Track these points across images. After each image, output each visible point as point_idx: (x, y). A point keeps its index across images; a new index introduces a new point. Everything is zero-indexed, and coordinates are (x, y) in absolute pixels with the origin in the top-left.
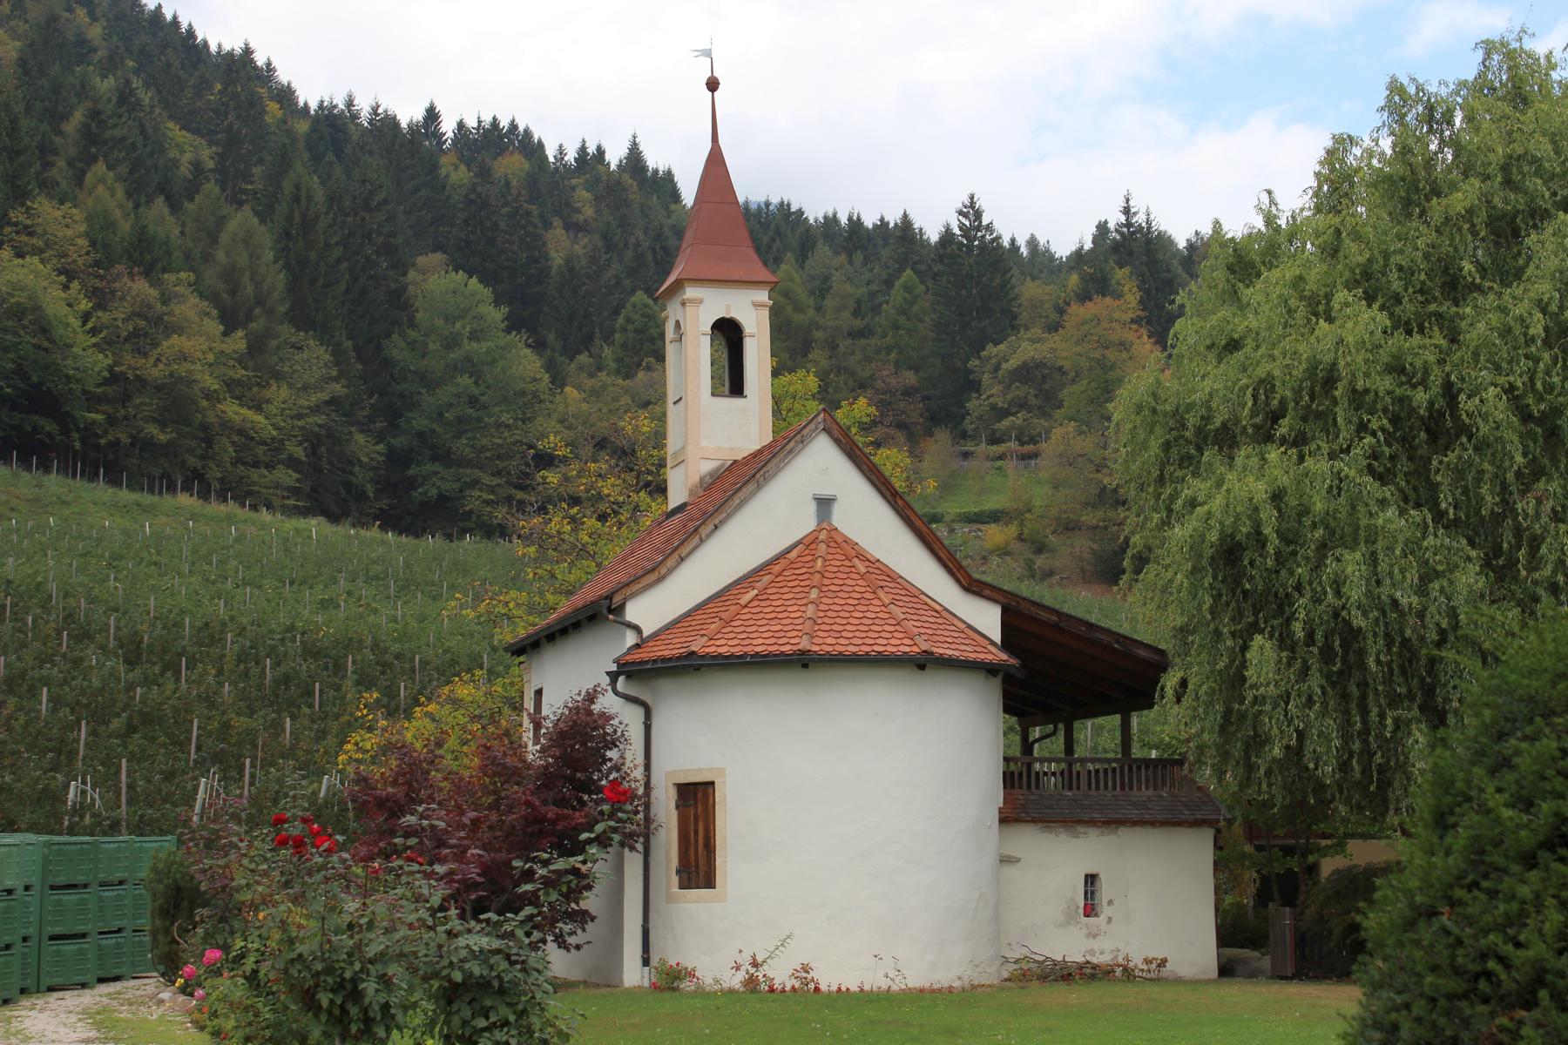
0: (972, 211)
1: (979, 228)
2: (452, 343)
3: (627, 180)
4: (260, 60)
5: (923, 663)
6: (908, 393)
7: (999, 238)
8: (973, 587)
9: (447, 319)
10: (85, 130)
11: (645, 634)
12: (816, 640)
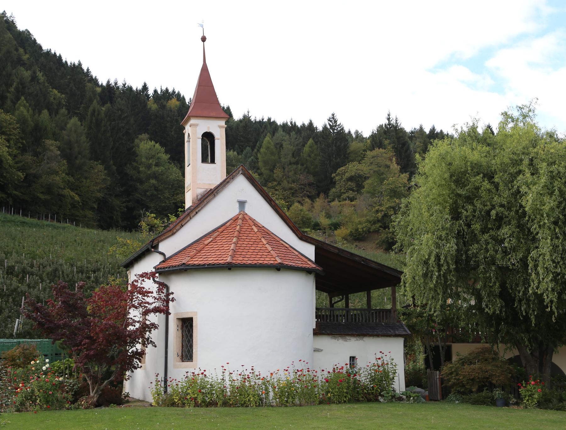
0: (333, 119)
2: (149, 167)
4: (85, 68)
5: (279, 268)
6: (310, 185)
7: (343, 129)
8: (303, 238)
9: (147, 159)
10: (17, 89)
12: (235, 258)
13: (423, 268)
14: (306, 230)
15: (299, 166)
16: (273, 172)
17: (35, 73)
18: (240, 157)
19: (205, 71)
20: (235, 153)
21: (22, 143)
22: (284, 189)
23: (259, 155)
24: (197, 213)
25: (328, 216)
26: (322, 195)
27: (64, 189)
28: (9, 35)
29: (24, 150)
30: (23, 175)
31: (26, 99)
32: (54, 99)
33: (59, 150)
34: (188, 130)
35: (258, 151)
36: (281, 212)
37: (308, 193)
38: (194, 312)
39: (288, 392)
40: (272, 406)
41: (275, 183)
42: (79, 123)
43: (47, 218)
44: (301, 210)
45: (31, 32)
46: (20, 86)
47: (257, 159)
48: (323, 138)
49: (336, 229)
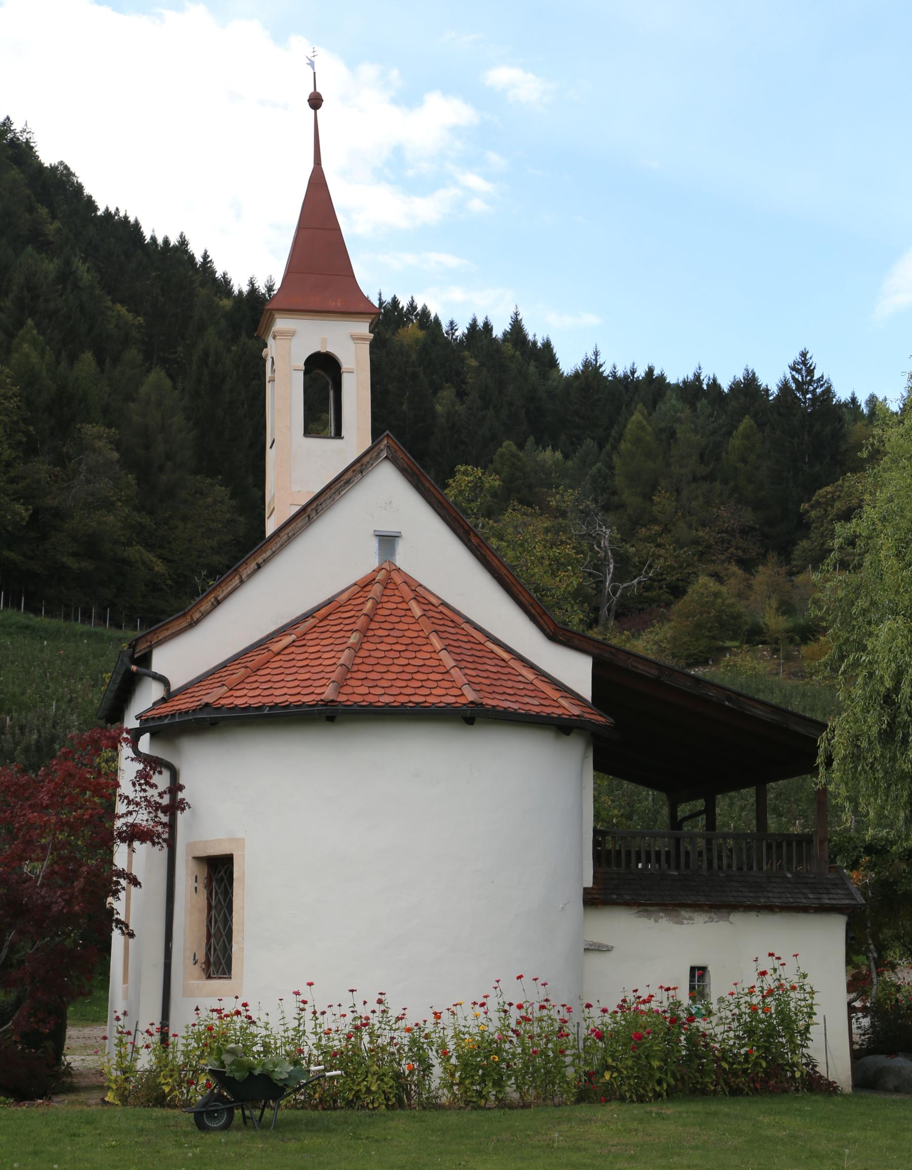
0: (803, 365)
1: (811, 382)
3: (509, 348)
5: (471, 716)
6: (745, 532)
7: (828, 392)
8: (558, 635)
11: (174, 687)
13: (880, 715)
14: (728, 644)
15: (718, 486)
16: (651, 500)
17: (68, 263)
18: (570, 463)
19: (318, 185)
20: (558, 455)
21: (26, 434)
22: (680, 544)
23: (616, 459)
24: (259, 567)
25: (786, 608)
26: (773, 557)
27: (129, 543)
28: (15, 173)
29: (30, 450)
30: (27, 510)
31: (38, 325)
32: (117, 326)
33: (117, 450)
34: (273, 349)
35: (615, 448)
36: (495, 563)
37: (740, 553)
38: (237, 840)
39: (482, 1067)
40: (440, 1107)
41: (656, 528)
42: (168, 383)
43: (87, 616)
44: (716, 595)
45: (73, 169)
46: (26, 293)
47: (611, 468)
48: (780, 414)
49: (805, 640)
